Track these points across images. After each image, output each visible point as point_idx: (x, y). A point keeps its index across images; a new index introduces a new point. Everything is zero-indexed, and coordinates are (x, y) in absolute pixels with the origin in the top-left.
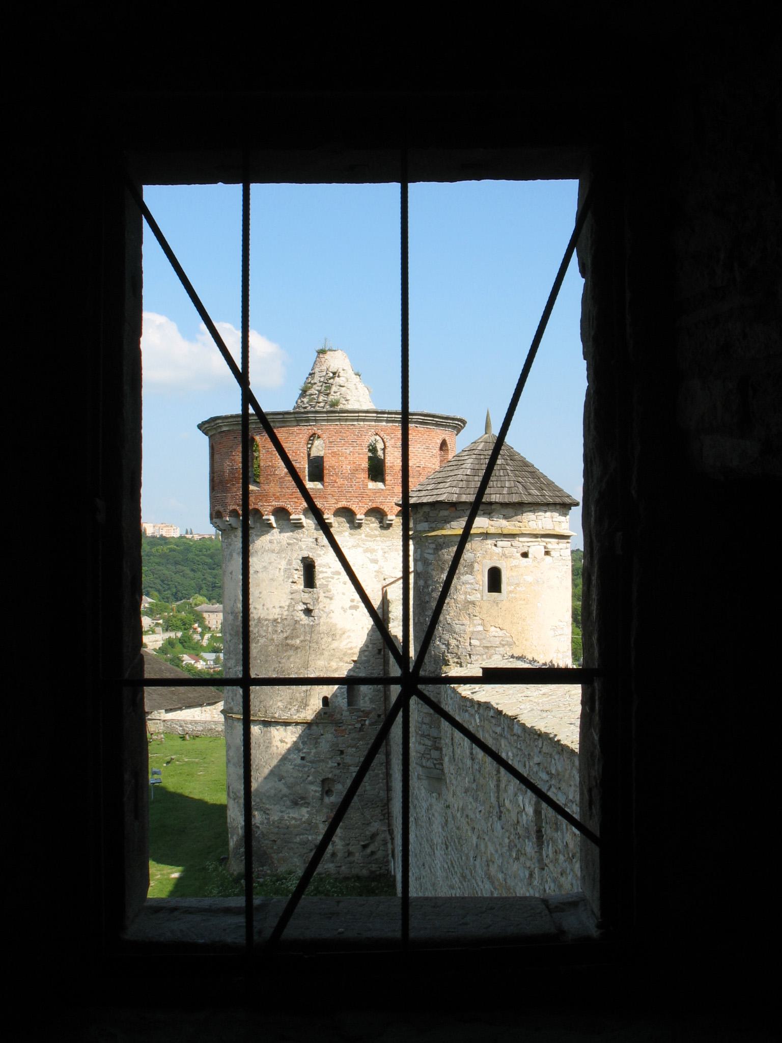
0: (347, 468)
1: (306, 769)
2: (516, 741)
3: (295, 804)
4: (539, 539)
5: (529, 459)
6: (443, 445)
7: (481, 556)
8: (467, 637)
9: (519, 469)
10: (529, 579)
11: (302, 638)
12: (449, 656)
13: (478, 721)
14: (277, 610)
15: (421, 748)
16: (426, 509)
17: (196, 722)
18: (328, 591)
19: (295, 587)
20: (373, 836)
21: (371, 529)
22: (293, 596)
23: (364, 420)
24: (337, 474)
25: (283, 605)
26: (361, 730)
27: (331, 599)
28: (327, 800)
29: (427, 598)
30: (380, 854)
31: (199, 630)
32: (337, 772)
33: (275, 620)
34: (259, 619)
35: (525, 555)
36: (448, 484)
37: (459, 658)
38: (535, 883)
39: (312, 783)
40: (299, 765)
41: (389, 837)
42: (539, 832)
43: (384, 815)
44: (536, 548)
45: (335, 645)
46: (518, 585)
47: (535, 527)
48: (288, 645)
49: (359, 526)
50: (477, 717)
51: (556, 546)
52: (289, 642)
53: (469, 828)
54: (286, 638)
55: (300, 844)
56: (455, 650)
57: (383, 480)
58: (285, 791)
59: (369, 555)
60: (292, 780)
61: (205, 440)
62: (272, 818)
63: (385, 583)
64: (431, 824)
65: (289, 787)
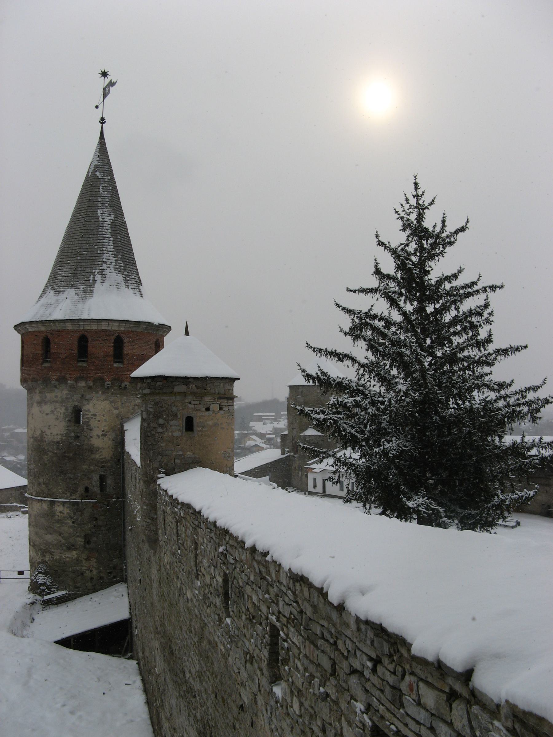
10: (210, 423)
13: (182, 514)
14: (59, 437)
18: (90, 425)
20: (114, 568)
27: (91, 430)
32: (93, 530)
35: (208, 409)
39: (78, 536)
46: (203, 427)
48: (65, 456)
51: (226, 404)
54: (64, 452)
57: (122, 362)
60: (66, 535)
62: (55, 558)
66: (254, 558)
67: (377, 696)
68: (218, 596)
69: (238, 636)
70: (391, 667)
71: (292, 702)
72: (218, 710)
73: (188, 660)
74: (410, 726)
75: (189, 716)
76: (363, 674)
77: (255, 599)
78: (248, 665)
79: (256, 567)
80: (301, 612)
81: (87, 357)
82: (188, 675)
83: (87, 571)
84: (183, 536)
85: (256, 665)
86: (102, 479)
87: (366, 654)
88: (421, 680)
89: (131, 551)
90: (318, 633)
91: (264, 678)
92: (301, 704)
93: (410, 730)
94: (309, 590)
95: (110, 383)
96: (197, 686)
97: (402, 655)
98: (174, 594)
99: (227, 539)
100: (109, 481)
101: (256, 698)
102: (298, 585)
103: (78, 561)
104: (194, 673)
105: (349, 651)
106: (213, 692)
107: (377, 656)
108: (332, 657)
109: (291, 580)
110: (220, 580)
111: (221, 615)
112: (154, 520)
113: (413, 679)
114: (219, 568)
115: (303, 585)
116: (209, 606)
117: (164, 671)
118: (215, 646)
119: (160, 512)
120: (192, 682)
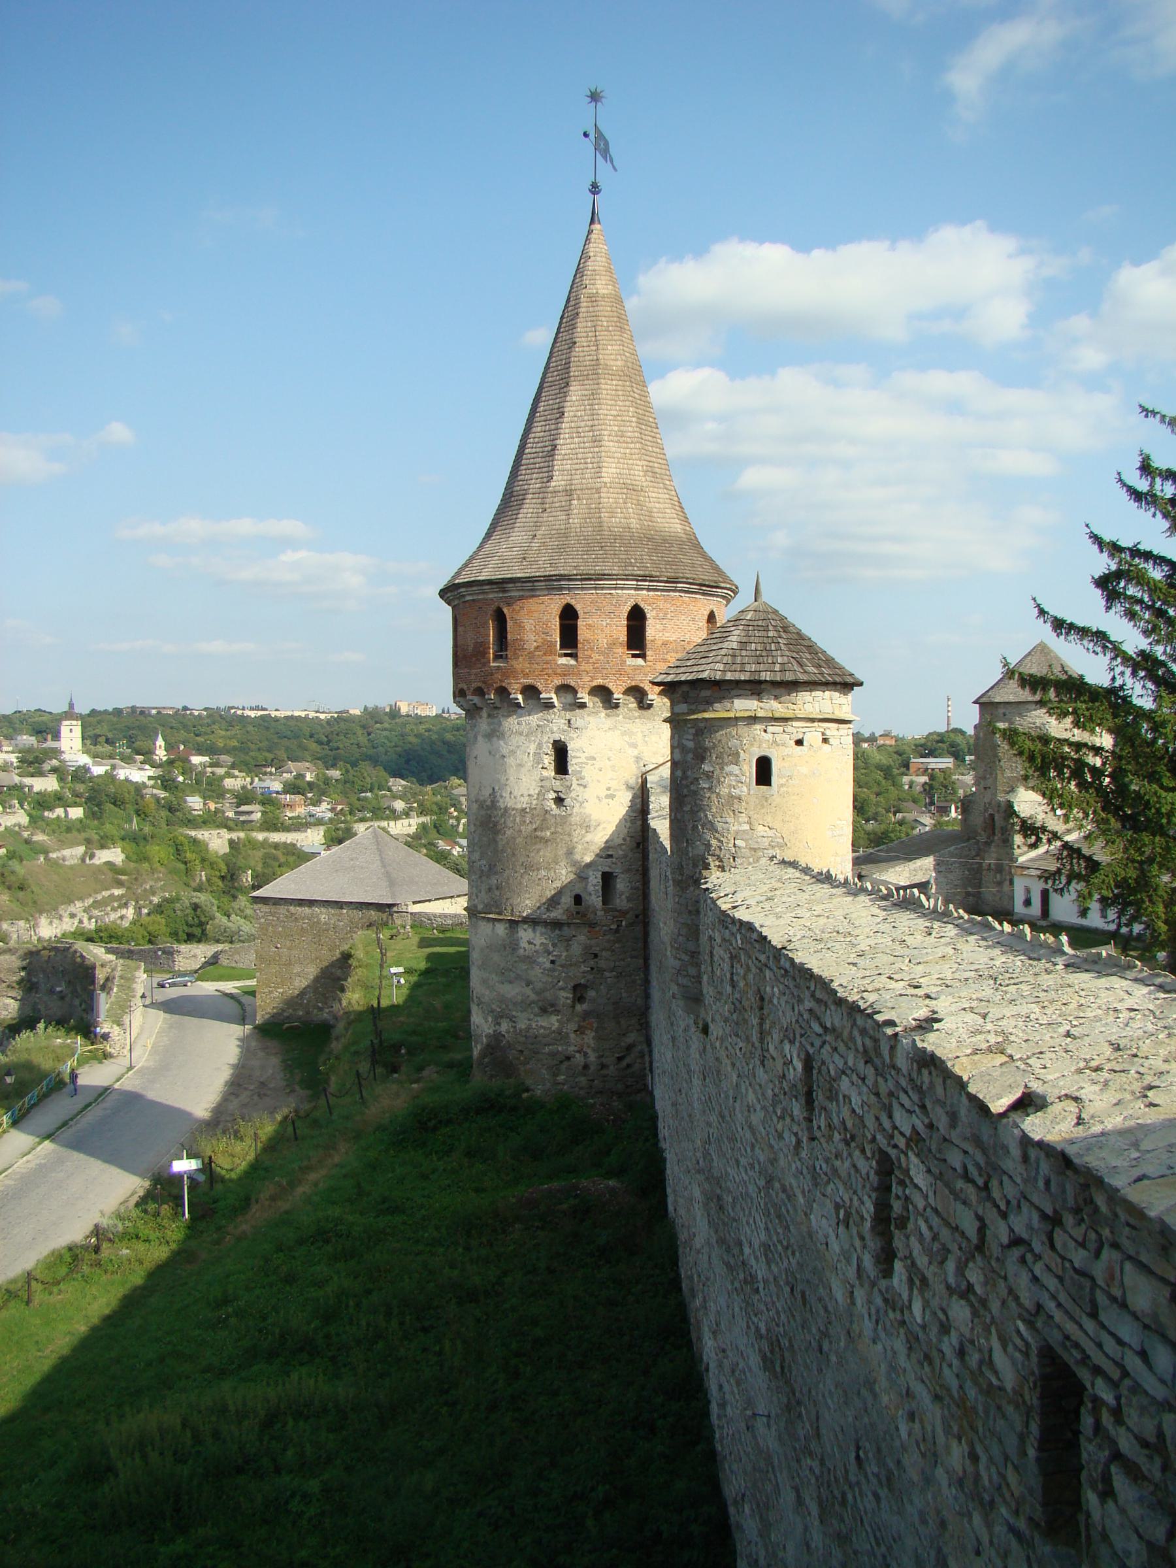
0: (603, 642)
1: (556, 974)
2: (783, 976)
3: (544, 1011)
4: (816, 724)
5: (806, 631)
6: (711, 618)
7: (756, 742)
8: (731, 837)
9: (793, 642)
10: (804, 770)
11: (553, 829)
12: (710, 859)
14: (526, 799)
15: (677, 964)
16: (685, 688)
17: (445, 916)
19: (545, 773)
20: (629, 1048)
21: (630, 710)
22: (544, 783)
23: (622, 588)
24: (592, 649)
25: (532, 792)
26: (617, 931)
27: (585, 787)
28: (579, 1007)
29: (685, 791)
30: (637, 1066)
31: (455, 814)
32: (590, 977)
33: (524, 810)
34: (506, 809)
35: (799, 742)
36: (710, 660)
37: (721, 861)
38: (803, 1154)
39: (562, 989)
40: (549, 970)
41: (646, 1050)
42: (809, 1094)
43: (641, 1025)
44: (813, 735)
45: (589, 837)
46: (790, 777)
47: (811, 710)
49: (617, 706)
50: (739, 937)
51: (835, 733)
52: (539, 833)
53: (729, 1062)
55: (548, 1054)
56: (717, 852)
57: (643, 656)
58: (533, 997)
59: (627, 738)
60: (539, 985)
61: (447, 612)
63: (644, 770)
64: (688, 1047)
65: (537, 993)
66: (854, 1024)
67: (1052, 1289)
68: (796, 1097)
69: (826, 1174)
70: (1078, 1233)
71: (910, 1301)
72: (793, 1316)
73: (748, 1223)
74: (1106, 1349)
75: (748, 1327)
76: (1030, 1245)
77: (856, 1101)
78: (841, 1229)
79: (859, 1040)
80: (931, 1126)
81: (576, 646)
82: (747, 1250)
83: (578, 1055)
84: (742, 984)
85: (854, 1231)
86: (607, 878)
87: (1037, 1208)
88: (1130, 1258)
89: (657, 1017)
90: (958, 1166)
91: (866, 1252)
92: (926, 1305)
93: (1107, 1355)
94: (944, 1082)
95: (621, 696)
96: (760, 1270)
97: (1096, 1210)
98: (727, 1097)
99: (812, 988)
100: (621, 885)
101: (852, 1292)
102: (925, 1072)
103: (561, 1036)
104: (756, 1247)
105: (1008, 1202)
106: (787, 1283)
107: (1055, 1211)
108: (980, 1212)
109: (915, 1065)
110: (799, 1065)
111: (800, 1133)
112: (694, 954)
113: (1116, 1255)
114: (797, 1044)
115: (934, 1074)
116: (782, 1118)
117: (708, 1243)
118: (791, 1197)
119: (704, 939)
120: (753, 1262)
